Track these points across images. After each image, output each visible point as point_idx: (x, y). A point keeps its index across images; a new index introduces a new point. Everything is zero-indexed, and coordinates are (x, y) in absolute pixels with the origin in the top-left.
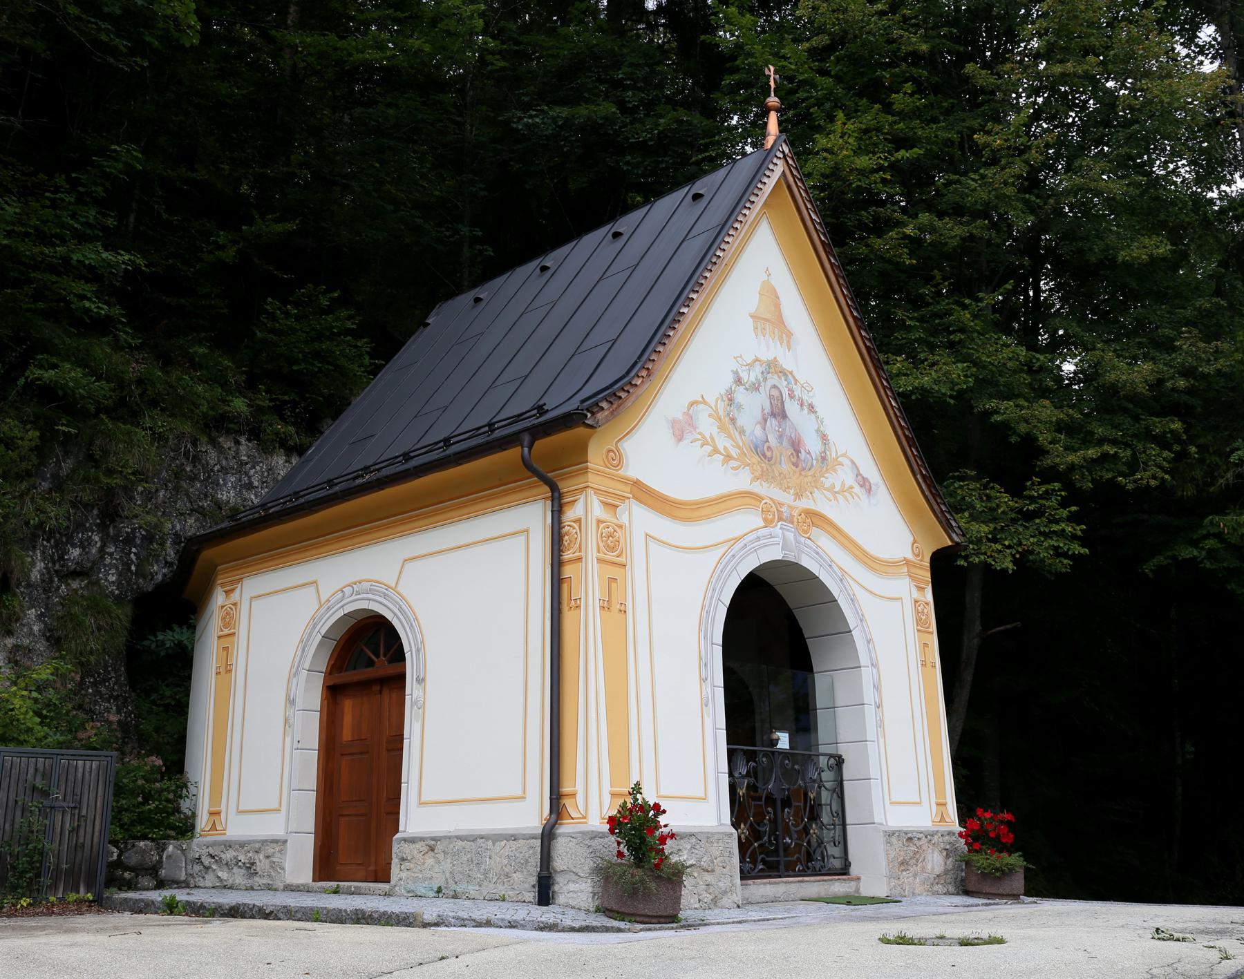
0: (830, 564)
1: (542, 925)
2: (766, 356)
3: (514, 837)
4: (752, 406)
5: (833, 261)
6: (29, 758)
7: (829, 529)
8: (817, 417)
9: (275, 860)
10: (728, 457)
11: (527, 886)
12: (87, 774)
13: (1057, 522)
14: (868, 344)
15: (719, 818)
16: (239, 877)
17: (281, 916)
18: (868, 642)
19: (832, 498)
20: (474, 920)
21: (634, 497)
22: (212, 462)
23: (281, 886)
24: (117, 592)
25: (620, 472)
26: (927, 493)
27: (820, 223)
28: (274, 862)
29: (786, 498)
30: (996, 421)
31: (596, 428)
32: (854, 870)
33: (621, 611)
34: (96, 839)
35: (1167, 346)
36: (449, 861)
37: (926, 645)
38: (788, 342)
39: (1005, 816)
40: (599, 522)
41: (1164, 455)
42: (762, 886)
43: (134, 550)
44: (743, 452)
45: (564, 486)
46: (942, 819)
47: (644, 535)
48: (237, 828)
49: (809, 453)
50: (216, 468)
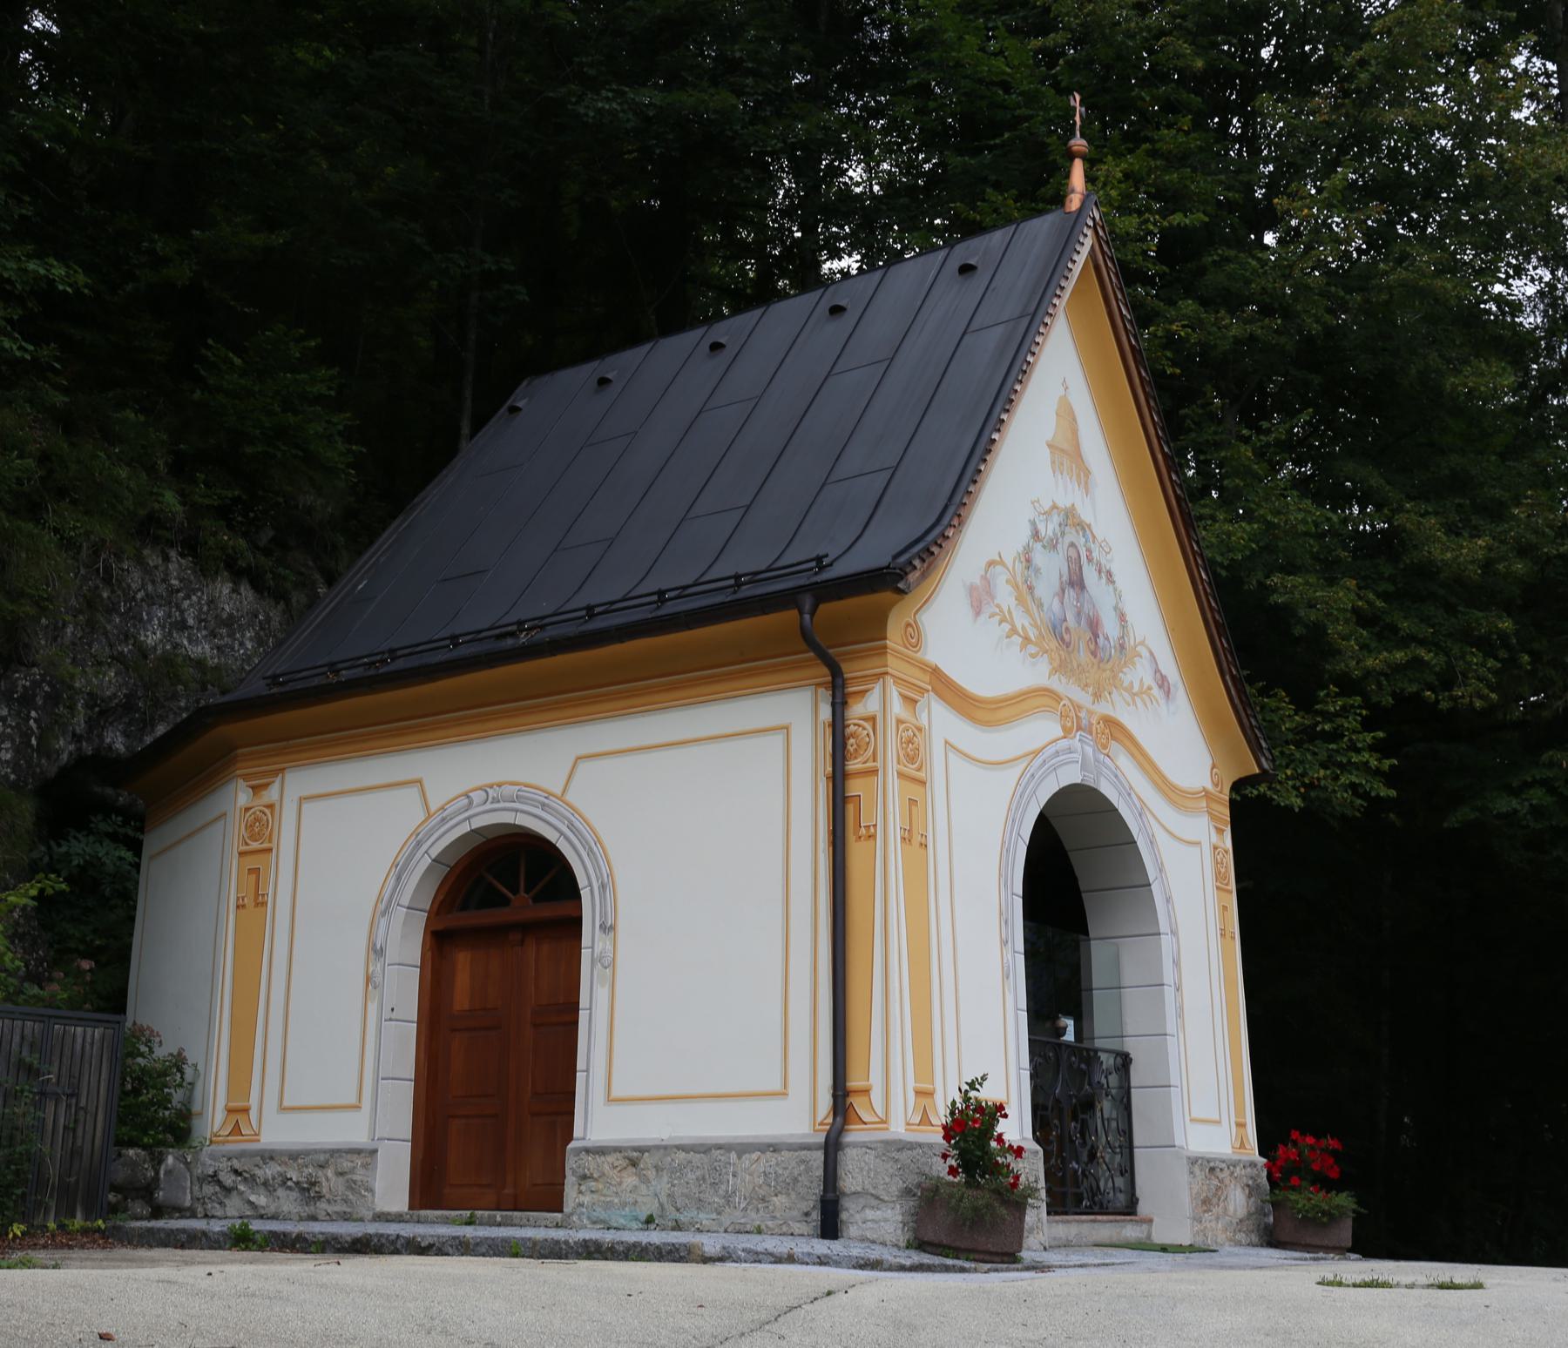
0: (1129, 792)
1: (862, 1262)
2: (1064, 502)
3: (775, 1148)
4: (1051, 566)
5: (1144, 374)
6: (13, 1019)
7: (1128, 743)
8: (1115, 590)
9: (355, 1177)
10: (1026, 639)
11: (795, 1213)
12: (88, 1047)
13: (1358, 751)
14: (1179, 492)
15: (1022, 1131)
16: (288, 1202)
17: (451, 1251)
18: (1168, 901)
19: (1129, 700)
20: (771, 1254)
21: (937, 693)
22: (134, 586)
23: (369, 1215)
24: (13, 777)
25: (919, 655)
26: (1237, 701)
27: (1130, 322)
28: (355, 1182)
29: (1083, 698)
30: (1276, 603)
31: (906, 593)
32: (1143, 1208)
33: (921, 844)
34: (98, 1142)
35: (1497, 512)
36: (665, 1179)
37: (1225, 908)
38: (1086, 483)
39: (1330, 1142)
40: (899, 722)
41: (1489, 665)
42: (1054, 1224)
43: (33, 714)
44: (1040, 633)
45: (850, 670)
46: (1242, 1146)
47: (943, 741)
48: (277, 1132)
49: (1107, 638)
50: (139, 596)
